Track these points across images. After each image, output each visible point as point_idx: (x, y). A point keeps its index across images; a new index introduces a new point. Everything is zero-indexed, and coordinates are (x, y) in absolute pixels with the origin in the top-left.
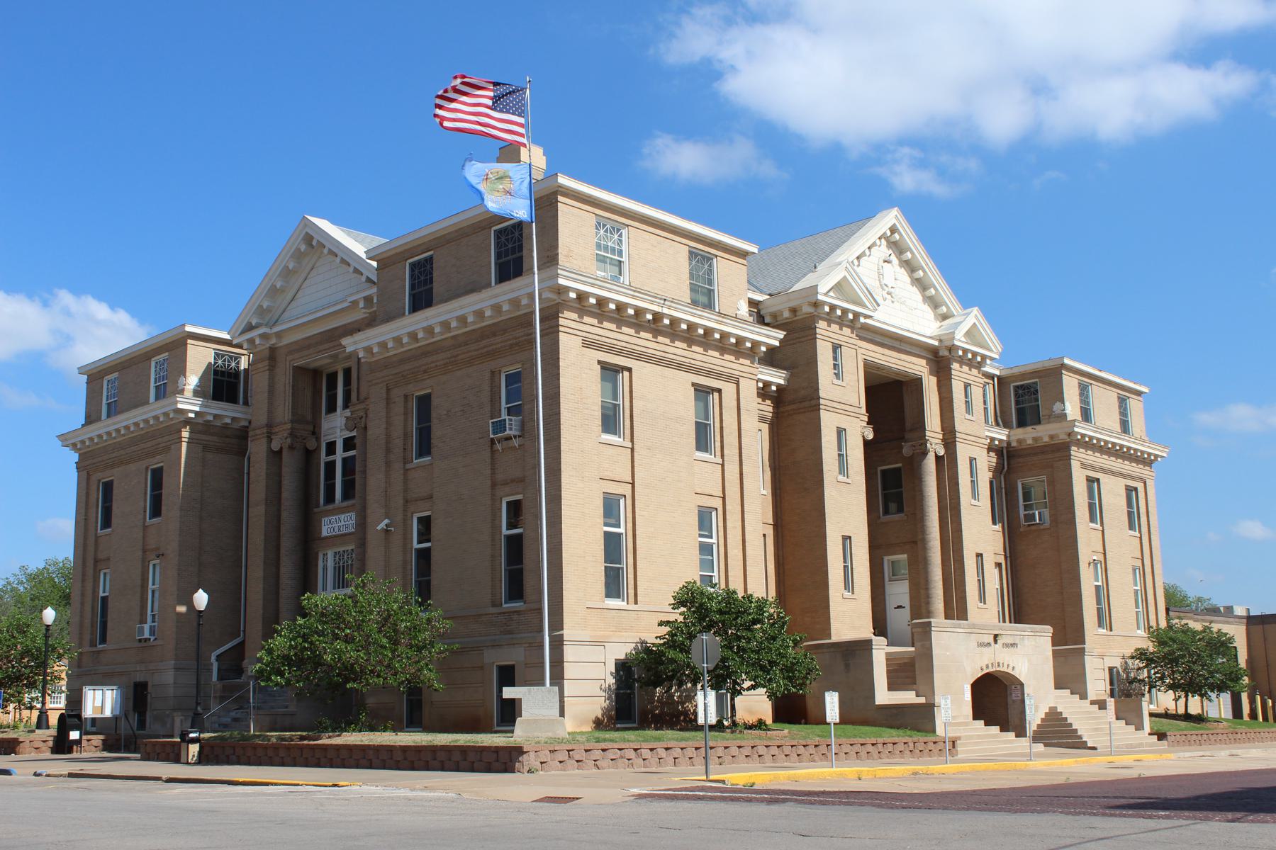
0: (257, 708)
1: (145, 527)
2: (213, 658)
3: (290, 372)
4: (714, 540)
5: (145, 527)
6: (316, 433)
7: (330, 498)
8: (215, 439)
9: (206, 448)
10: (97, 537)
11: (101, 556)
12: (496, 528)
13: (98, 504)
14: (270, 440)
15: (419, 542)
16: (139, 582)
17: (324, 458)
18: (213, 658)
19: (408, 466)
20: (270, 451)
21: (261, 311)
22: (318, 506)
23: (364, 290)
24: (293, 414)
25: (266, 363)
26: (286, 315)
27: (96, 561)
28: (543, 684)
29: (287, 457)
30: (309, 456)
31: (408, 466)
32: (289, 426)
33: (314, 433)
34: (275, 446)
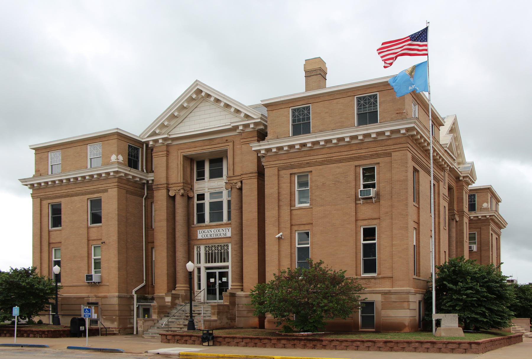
0: (356, 307)
1: (88, 228)
2: (134, 293)
3: (181, 159)
4: (229, 264)
5: (88, 228)
6: (192, 189)
7: (201, 219)
8: (131, 188)
9: (127, 192)
10: (49, 231)
11: (52, 241)
12: (357, 240)
13: (51, 216)
14: (168, 191)
15: (364, 240)
16: (86, 255)
17: (196, 202)
18: (134, 293)
19: (292, 208)
20: (169, 196)
21: (163, 126)
22: (194, 224)
23: (244, 121)
24: (184, 179)
25: (165, 152)
26: (436, 127)
27: (49, 244)
28: (14, 336)
29: (178, 199)
30: (190, 199)
31: (292, 208)
32: (182, 184)
33: (191, 189)
34: (172, 194)
